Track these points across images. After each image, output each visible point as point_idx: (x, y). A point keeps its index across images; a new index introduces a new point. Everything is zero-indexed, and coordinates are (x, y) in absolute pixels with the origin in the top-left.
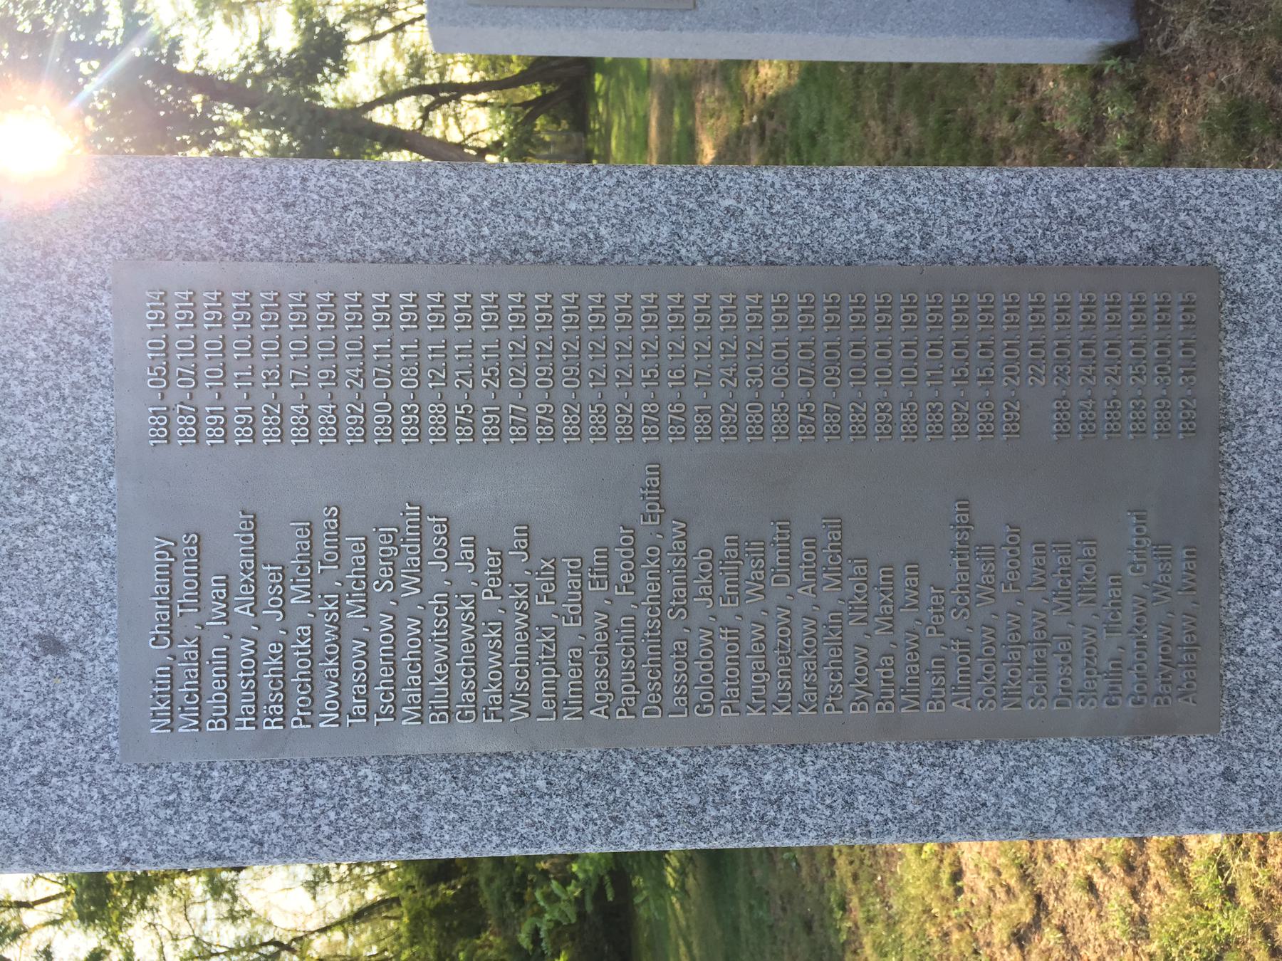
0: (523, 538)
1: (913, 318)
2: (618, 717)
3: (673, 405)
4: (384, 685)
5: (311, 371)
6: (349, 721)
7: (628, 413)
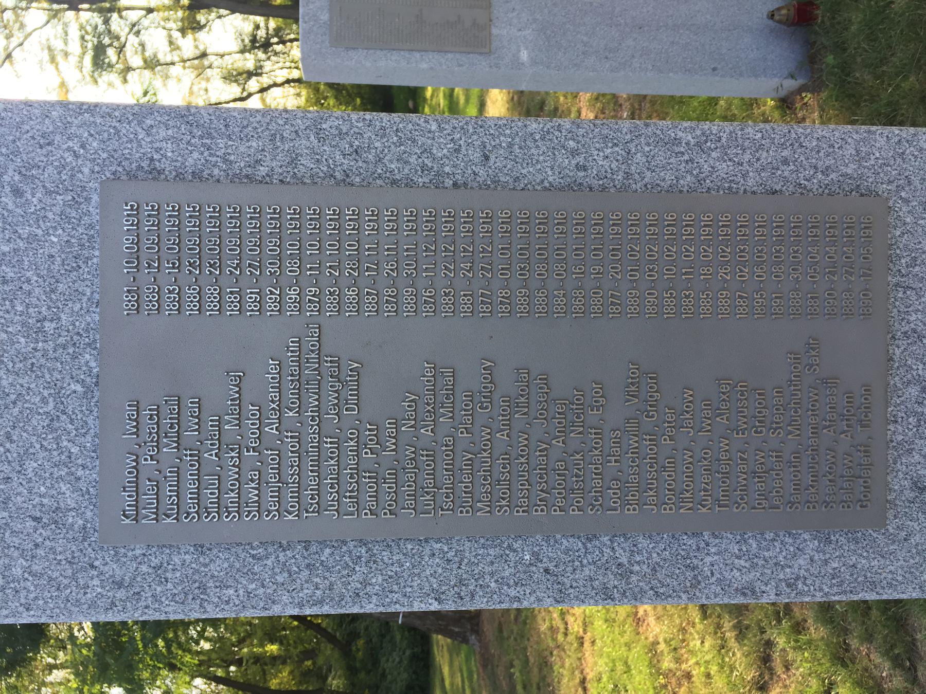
4: (311, 490)
6: (305, 515)
7: (276, 294)
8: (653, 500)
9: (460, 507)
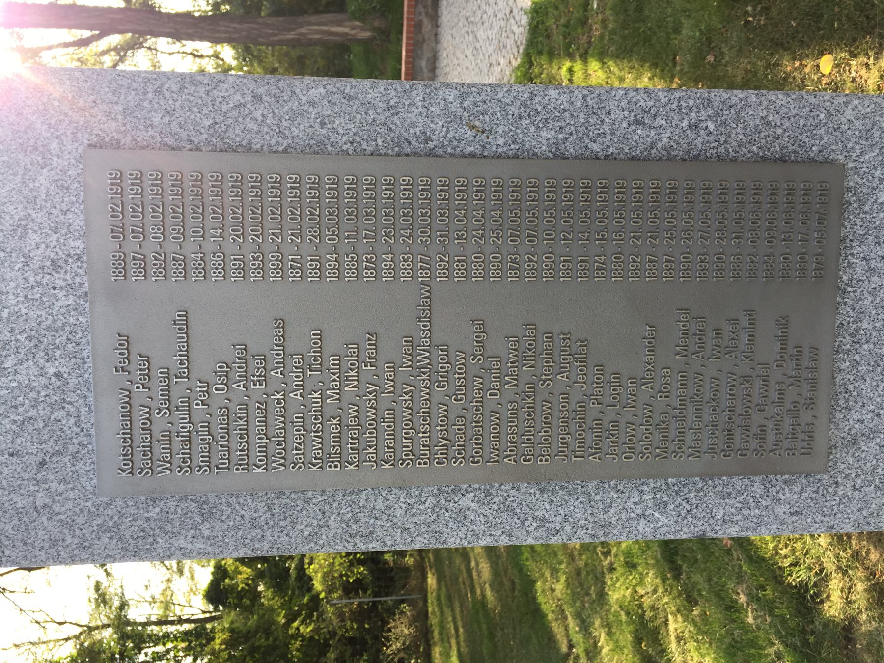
0: (409, 346)
1: (535, 197)
2: (235, 472)
3: (214, 254)
5: (225, 228)
8: (373, 457)
9: (237, 464)
